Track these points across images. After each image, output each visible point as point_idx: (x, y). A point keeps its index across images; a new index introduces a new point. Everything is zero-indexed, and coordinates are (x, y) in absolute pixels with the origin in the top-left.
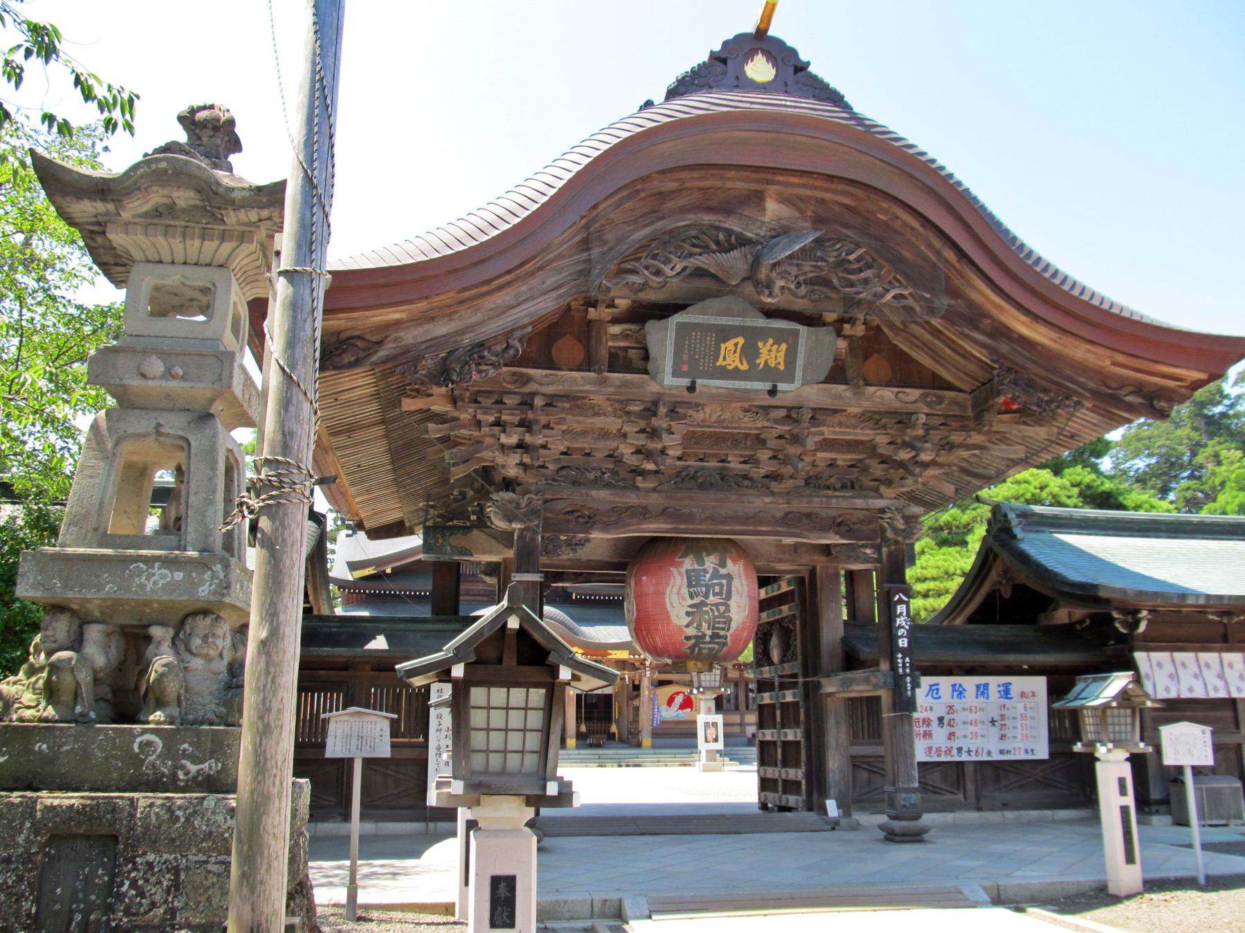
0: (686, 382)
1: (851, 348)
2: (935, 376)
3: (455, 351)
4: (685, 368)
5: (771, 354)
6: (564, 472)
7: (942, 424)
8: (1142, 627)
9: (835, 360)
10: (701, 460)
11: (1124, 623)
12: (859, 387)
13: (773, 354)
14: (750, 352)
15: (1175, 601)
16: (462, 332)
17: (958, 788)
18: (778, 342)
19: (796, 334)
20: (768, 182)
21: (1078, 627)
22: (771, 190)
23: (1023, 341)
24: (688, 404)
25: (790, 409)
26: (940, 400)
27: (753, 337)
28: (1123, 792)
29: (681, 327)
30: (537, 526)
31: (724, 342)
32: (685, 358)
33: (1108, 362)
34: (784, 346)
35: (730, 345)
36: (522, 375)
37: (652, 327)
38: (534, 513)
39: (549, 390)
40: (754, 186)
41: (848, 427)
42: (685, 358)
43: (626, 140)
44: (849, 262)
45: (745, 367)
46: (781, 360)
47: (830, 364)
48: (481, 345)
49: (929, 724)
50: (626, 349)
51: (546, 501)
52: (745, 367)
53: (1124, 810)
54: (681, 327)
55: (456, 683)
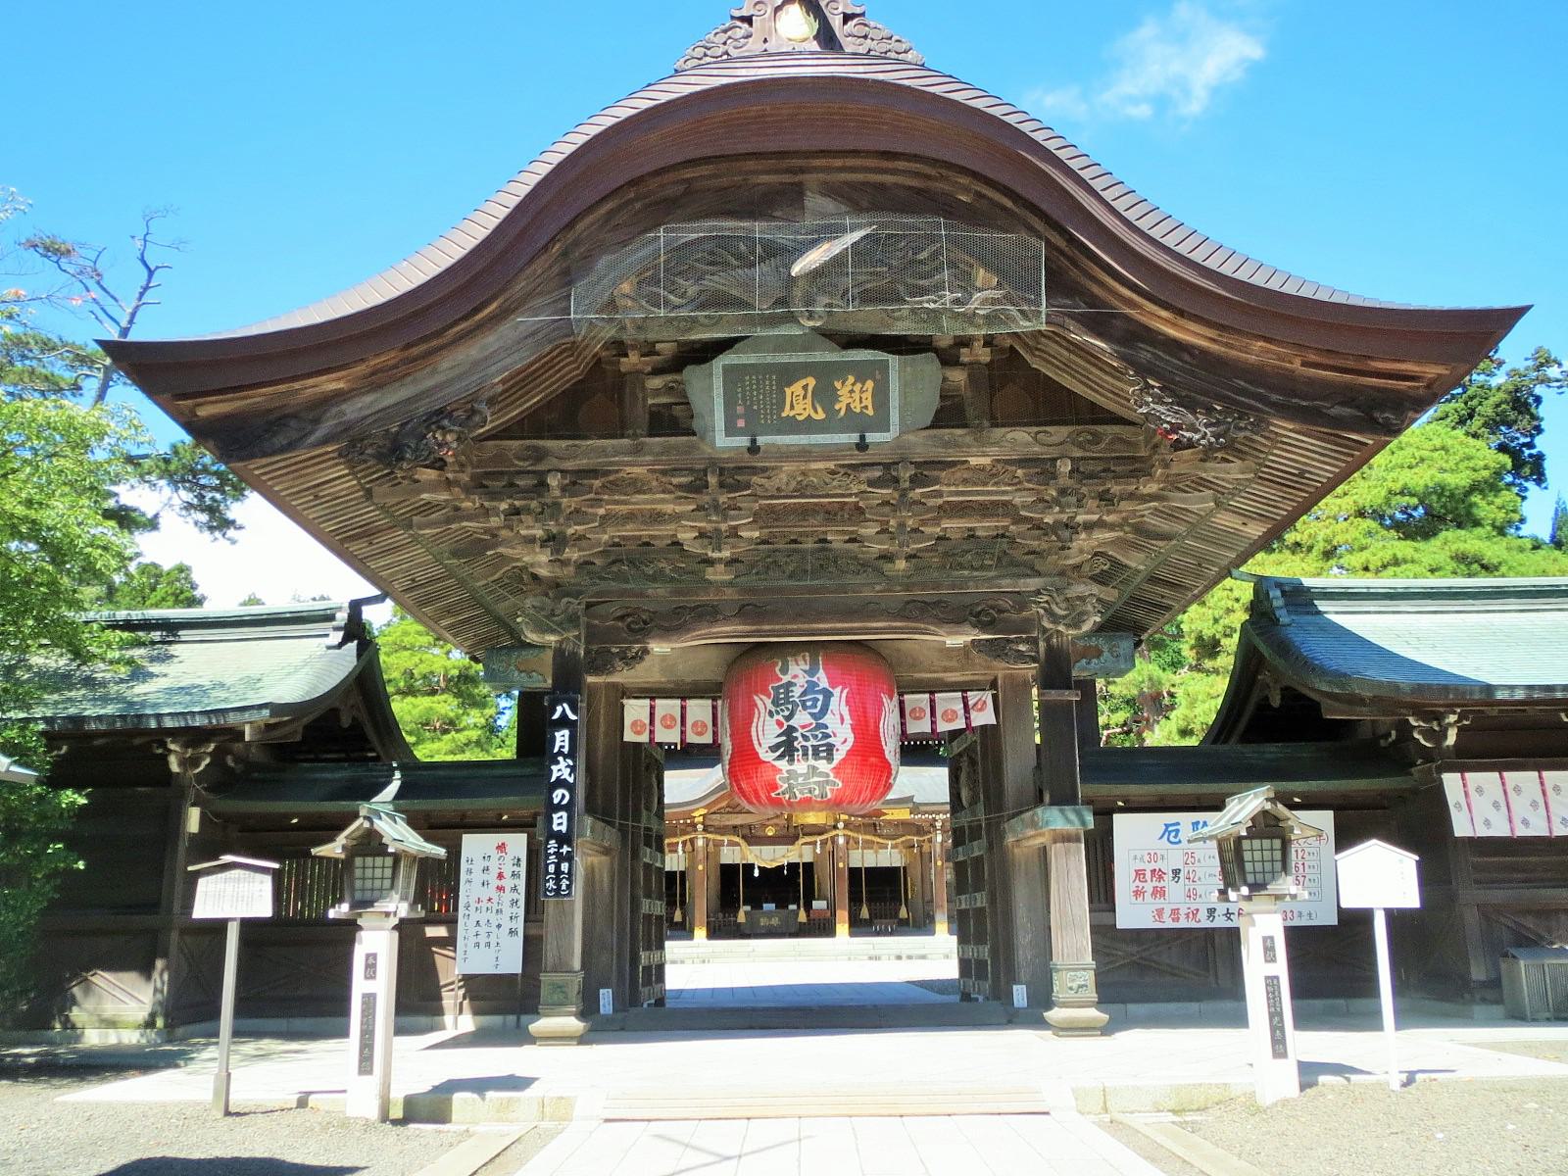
0: (743, 441)
1: (972, 379)
2: (1093, 406)
3: (407, 423)
4: (741, 423)
5: (853, 395)
6: (615, 569)
7: (1104, 471)
8: (1451, 738)
9: (942, 397)
10: (795, 541)
11: (1428, 734)
12: (983, 429)
13: (856, 396)
14: (825, 395)
15: (1477, 696)
16: (417, 397)
17: (1207, 969)
18: (861, 379)
19: (884, 366)
20: (802, 170)
21: (1382, 743)
22: (810, 179)
23: (1176, 346)
24: (754, 471)
25: (887, 466)
26: (1097, 439)
27: (826, 375)
28: (1270, 957)
29: (728, 370)
30: (578, 637)
31: (789, 385)
32: (740, 410)
33: (1298, 362)
34: (870, 384)
35: (797, 388)
36: (536, 449)
37: (692, 374)
38: (573, 620)
39: (569, 465)
40: (787, 178)
41: (975, 484)
42: (740, 410)
43: (596, 137)
44: (921, 262)
45: (821, 415)
46: (869, 403)
47: (936, 404)
48: (440, 412)
49: (1160, 878)
50: (669, 406)
51: (589, 605)
52: (821, 415)
53: (1272, 982)
54: (728, 370)
55: (444, 828)
